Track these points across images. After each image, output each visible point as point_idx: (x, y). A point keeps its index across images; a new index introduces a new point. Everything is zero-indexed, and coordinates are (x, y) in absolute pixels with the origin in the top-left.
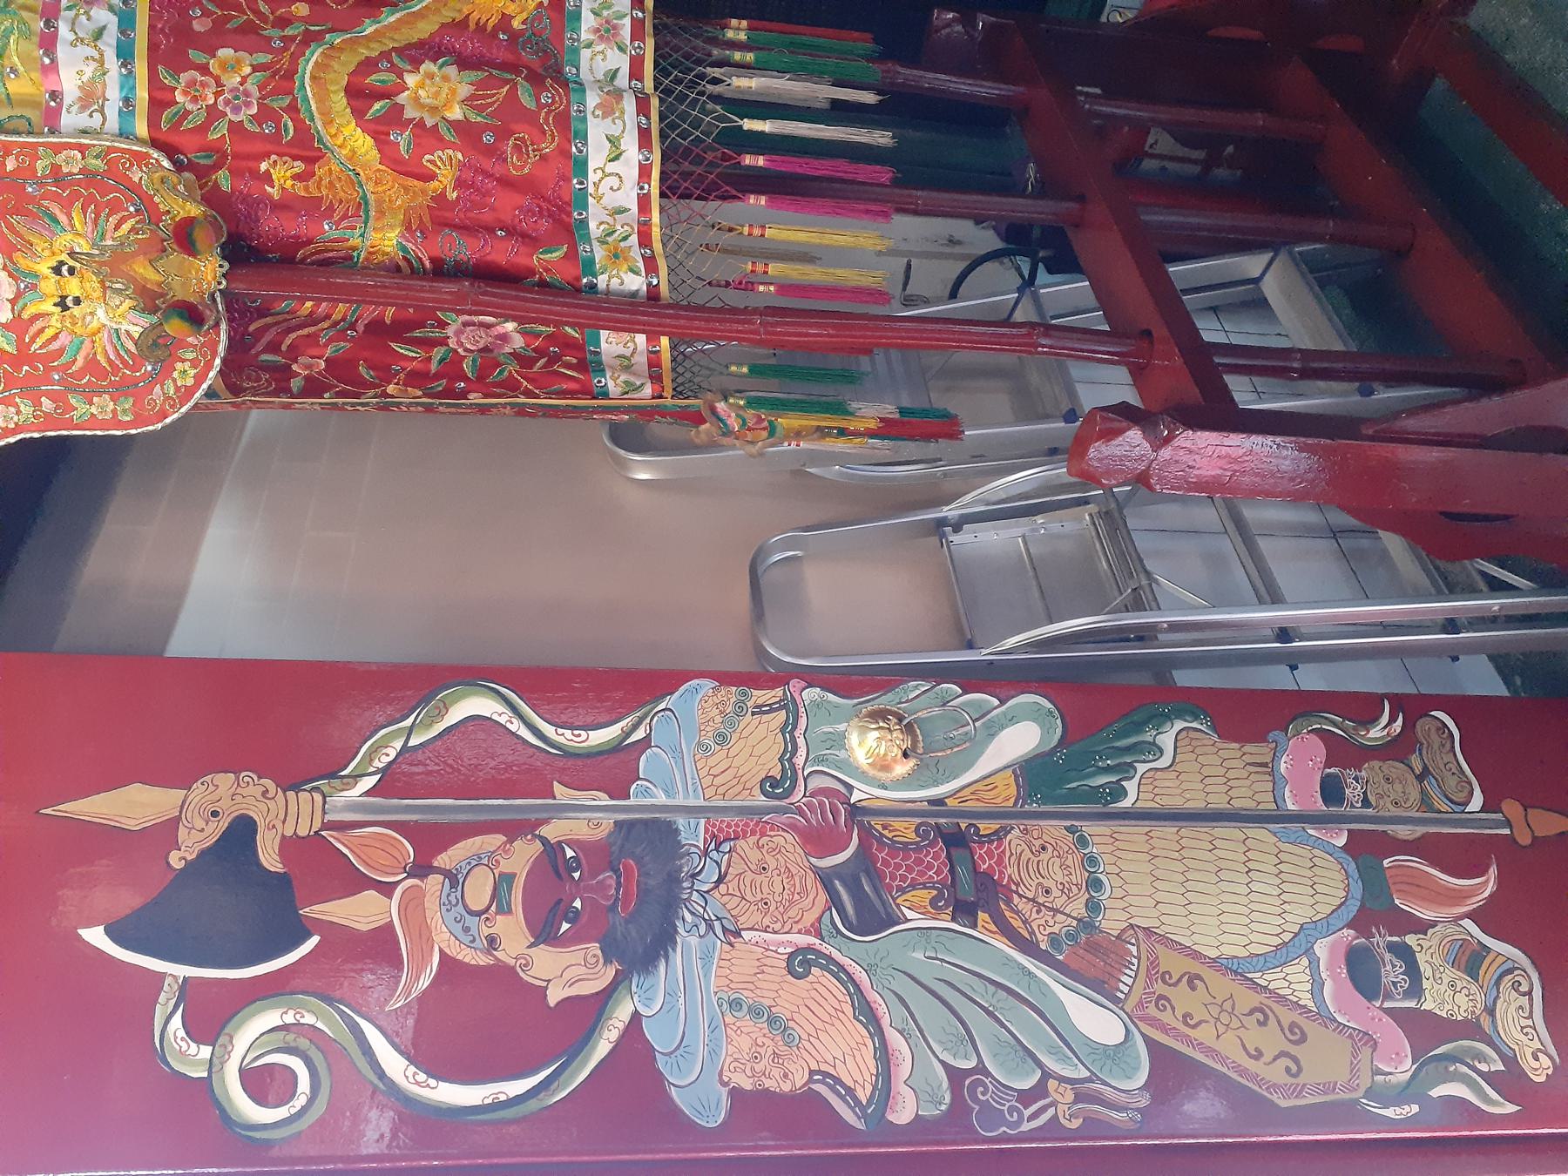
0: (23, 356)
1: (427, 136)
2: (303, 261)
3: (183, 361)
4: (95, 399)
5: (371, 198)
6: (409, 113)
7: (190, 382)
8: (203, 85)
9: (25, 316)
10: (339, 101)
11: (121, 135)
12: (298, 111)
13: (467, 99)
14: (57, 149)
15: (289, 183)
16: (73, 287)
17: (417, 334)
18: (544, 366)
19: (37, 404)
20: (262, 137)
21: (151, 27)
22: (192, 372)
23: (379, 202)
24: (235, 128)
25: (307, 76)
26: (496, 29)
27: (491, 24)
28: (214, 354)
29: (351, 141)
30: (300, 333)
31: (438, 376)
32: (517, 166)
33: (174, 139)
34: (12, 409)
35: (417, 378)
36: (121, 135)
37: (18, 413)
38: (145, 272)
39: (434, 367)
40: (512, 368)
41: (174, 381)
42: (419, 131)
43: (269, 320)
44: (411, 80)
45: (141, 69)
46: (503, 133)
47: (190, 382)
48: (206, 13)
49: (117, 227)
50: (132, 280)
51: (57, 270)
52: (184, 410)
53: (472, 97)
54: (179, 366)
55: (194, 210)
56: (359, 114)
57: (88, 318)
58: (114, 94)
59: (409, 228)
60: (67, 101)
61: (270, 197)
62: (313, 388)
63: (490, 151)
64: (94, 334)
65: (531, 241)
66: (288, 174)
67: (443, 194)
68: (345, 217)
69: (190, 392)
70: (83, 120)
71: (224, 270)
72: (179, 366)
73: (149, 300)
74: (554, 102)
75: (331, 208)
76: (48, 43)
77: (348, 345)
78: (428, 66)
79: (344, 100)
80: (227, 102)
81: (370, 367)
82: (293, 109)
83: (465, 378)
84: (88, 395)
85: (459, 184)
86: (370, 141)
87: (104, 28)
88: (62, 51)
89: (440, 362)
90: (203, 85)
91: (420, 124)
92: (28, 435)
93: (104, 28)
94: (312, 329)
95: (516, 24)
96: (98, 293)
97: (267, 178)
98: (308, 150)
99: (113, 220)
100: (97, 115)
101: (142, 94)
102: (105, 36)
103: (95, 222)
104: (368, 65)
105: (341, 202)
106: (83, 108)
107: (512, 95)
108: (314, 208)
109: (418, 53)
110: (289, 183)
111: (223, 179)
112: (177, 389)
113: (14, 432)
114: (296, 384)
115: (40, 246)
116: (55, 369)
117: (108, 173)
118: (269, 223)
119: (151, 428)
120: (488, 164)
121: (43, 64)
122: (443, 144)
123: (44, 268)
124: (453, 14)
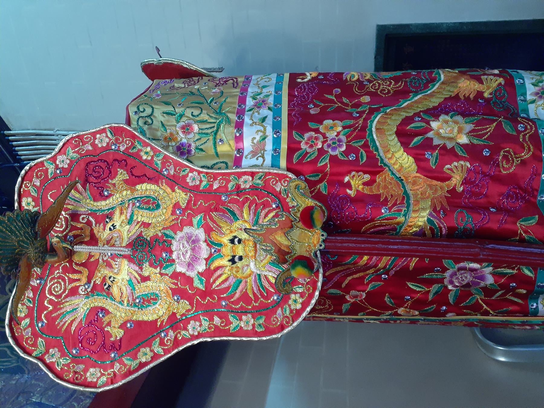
0: (208, 292)
1: (448, 153)
2: (365, 232)
3: (296, 293)
4: (244, 317)
5: (410, 193)
6: (436, 142)
7: (299, 306)
8: (316, 138)
9: (212, 268)
10: (394, 141)
11: (272, 167)
12: (369, 147)
13: (470, 132)
14: (240, 175)
15: (361, 187)
16: (240, 250)
17: (426, 276)
18: (500, 296)
19: (211, 319)
20: (349, 162)
21: (289, 115)
22: (300, 300)
23: (415, 195)
24: (333, 159)
25: (374, 129)
26: (476, 98)
27: (472, 96)
28: (315, 289)
29: (401, 160)
30: (355, 276)
31: (432, 303)
32: (507, 169)
33: (298, 168)
34: (198, 323)
35: (419, 304)
36: (272, 167)
37: (201, 325)
38: (281, 239)
39: (431, 297)
40: (479, 297)
41: (290, 306)
42: (442, 152)
43: (339, 268)
44: (434, 125)
45: (284, 134)
46: (495, 150)
47: (299, 306)
48: (316, 106)
49: (266, 216)
50: (274, 244)
51: (232, 241)
52: (295, 324)
53: (473, 131)
54: (293, 296)
55: (310, 202)
56: (405, 145)
57: (245, 268)
58: (269, 146)
59: (435, 210)
60: (246, 153)
61: (349, 196)
62: (355, 309)
63: (486, 161)
64: (247, 277)
65: (516, 215)
66: (360, 182)
67: (454, 188)
68: (395, 204)
69: (299, 313)
70: (254, 161)
71: (324, 238)
72: (293, 296)
73: (282, 256)
74: (526, 129)
75: (386, 201)
76: (239, 126)
77: (382, 283)
78: (443, 117)
79: (396, 139)
80: (329, 146)
81: (391, 297)
82: (366, 146)
83: (447, 304)
84: (240, 313)
85: (465, 182)
86: (411, 159)
87: (266, 117)
88: (245, 129)
89: (434, 294)
90: (316, 138)
91: (444, 147)
92: (205, 340)
93: (266, 117)
94: (361, 274)
95: (486, 95)
96: (252, 254)
97: (348, 185)
98: (374, 167)
99: (264, 213)
100: (261, 159)
101: (284, 146)
102: (267, 120)
103: (255, 214)
104: (408, 120)
105: (392, 196)
106: (253, 156)
107: (499, 125)
108: (377, 201)
109: (435, 113)
110: (361, 187)
111: (323, 187)
112: (291, 311)
113: (197, 337)
114: (345, 307)
115: (225, 228)
116: (224, 299)
117: (264, 188)
118: (350, 210)
119: (274, 336)
120: (486, 169)
121: (236, 136)
122: (459, 158)
123: (225, 240)
124: (450, 94)
